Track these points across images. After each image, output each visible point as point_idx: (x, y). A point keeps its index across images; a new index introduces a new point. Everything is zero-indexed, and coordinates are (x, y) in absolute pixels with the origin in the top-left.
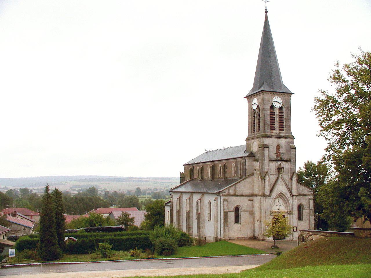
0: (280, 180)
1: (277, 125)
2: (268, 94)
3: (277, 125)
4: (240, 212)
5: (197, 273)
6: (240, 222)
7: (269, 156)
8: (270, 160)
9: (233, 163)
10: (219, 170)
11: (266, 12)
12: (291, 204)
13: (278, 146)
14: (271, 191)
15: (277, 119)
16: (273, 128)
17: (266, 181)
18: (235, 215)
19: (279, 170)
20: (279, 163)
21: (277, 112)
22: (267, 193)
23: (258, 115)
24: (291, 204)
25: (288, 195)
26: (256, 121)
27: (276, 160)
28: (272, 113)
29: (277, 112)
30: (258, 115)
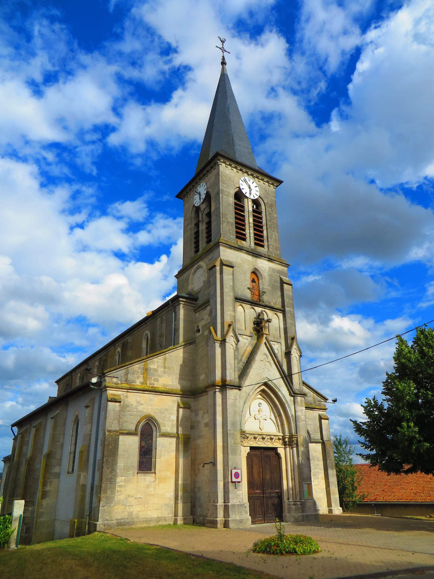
0: (263, 349)
1: (250, 232)
2: (229, 167)
3: (250, 232)
4: (154, 439)
5: (305, 528)
6: (153, 471)
7: (233, 287)
8: (239, 299)
9: (147, 332)
10: (116, 361)
11: (223, 63)
12: (292, 416)
13: (255, 272)
14: (243, 373)
15: (249, 220)
16: (241, 236)
17: (232, 294)
18: (141, 447)
19: (259, 326)
20: (259, 309)
21: (249, 206)
22: (232, 376)
23: (207, 215)
24: (292, 416)
25: (284, 391)
26: (203, 227)
27: (253, 303)
28: (239, 208)
29: (249, 206)
30: (207, 215)
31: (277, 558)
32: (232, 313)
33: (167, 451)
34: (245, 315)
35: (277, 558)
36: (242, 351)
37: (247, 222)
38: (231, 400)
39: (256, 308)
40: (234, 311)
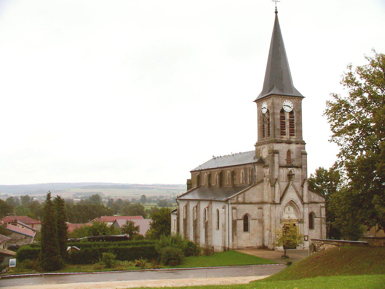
0: (291, 187)
1: (287, 130)
3: (287, 130)
4: (249, 221)
6: (249, 231)
7: (279, 162)
8: (281, 167)
9: (242, 170)
12: (302, 212)
14: (281, 199)
18: (244, 223)
19: (290, 176)
20: (290, 169)
21: (287, 117)
23: (268, 119)
24: (302, 212)
25: (299, 203)
27: (287, 167)
29: (287, 117)
31: (341, 147)
32: (278, 174)
33: (252, 224)
34: (284, 172)
35: (341, 147)
36: (282, 188)
37: (286, 125)
38: (266, 114)
39: (289, 168)
40: (279, 172)
